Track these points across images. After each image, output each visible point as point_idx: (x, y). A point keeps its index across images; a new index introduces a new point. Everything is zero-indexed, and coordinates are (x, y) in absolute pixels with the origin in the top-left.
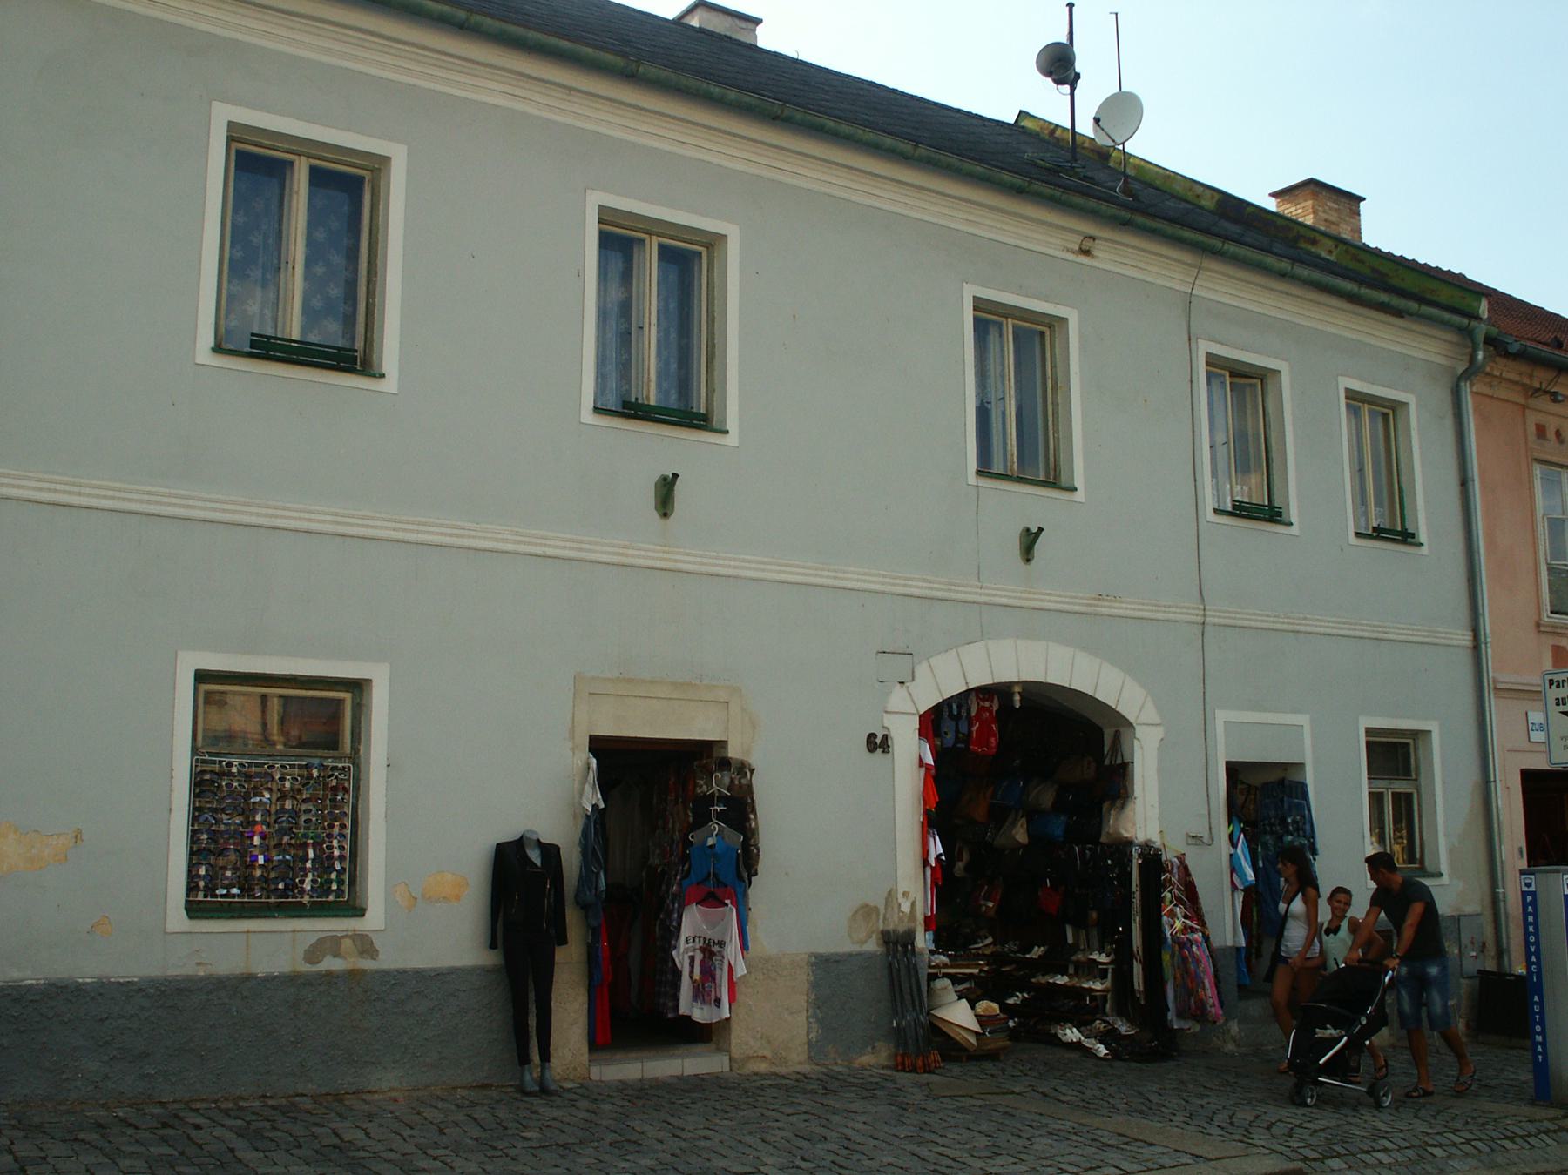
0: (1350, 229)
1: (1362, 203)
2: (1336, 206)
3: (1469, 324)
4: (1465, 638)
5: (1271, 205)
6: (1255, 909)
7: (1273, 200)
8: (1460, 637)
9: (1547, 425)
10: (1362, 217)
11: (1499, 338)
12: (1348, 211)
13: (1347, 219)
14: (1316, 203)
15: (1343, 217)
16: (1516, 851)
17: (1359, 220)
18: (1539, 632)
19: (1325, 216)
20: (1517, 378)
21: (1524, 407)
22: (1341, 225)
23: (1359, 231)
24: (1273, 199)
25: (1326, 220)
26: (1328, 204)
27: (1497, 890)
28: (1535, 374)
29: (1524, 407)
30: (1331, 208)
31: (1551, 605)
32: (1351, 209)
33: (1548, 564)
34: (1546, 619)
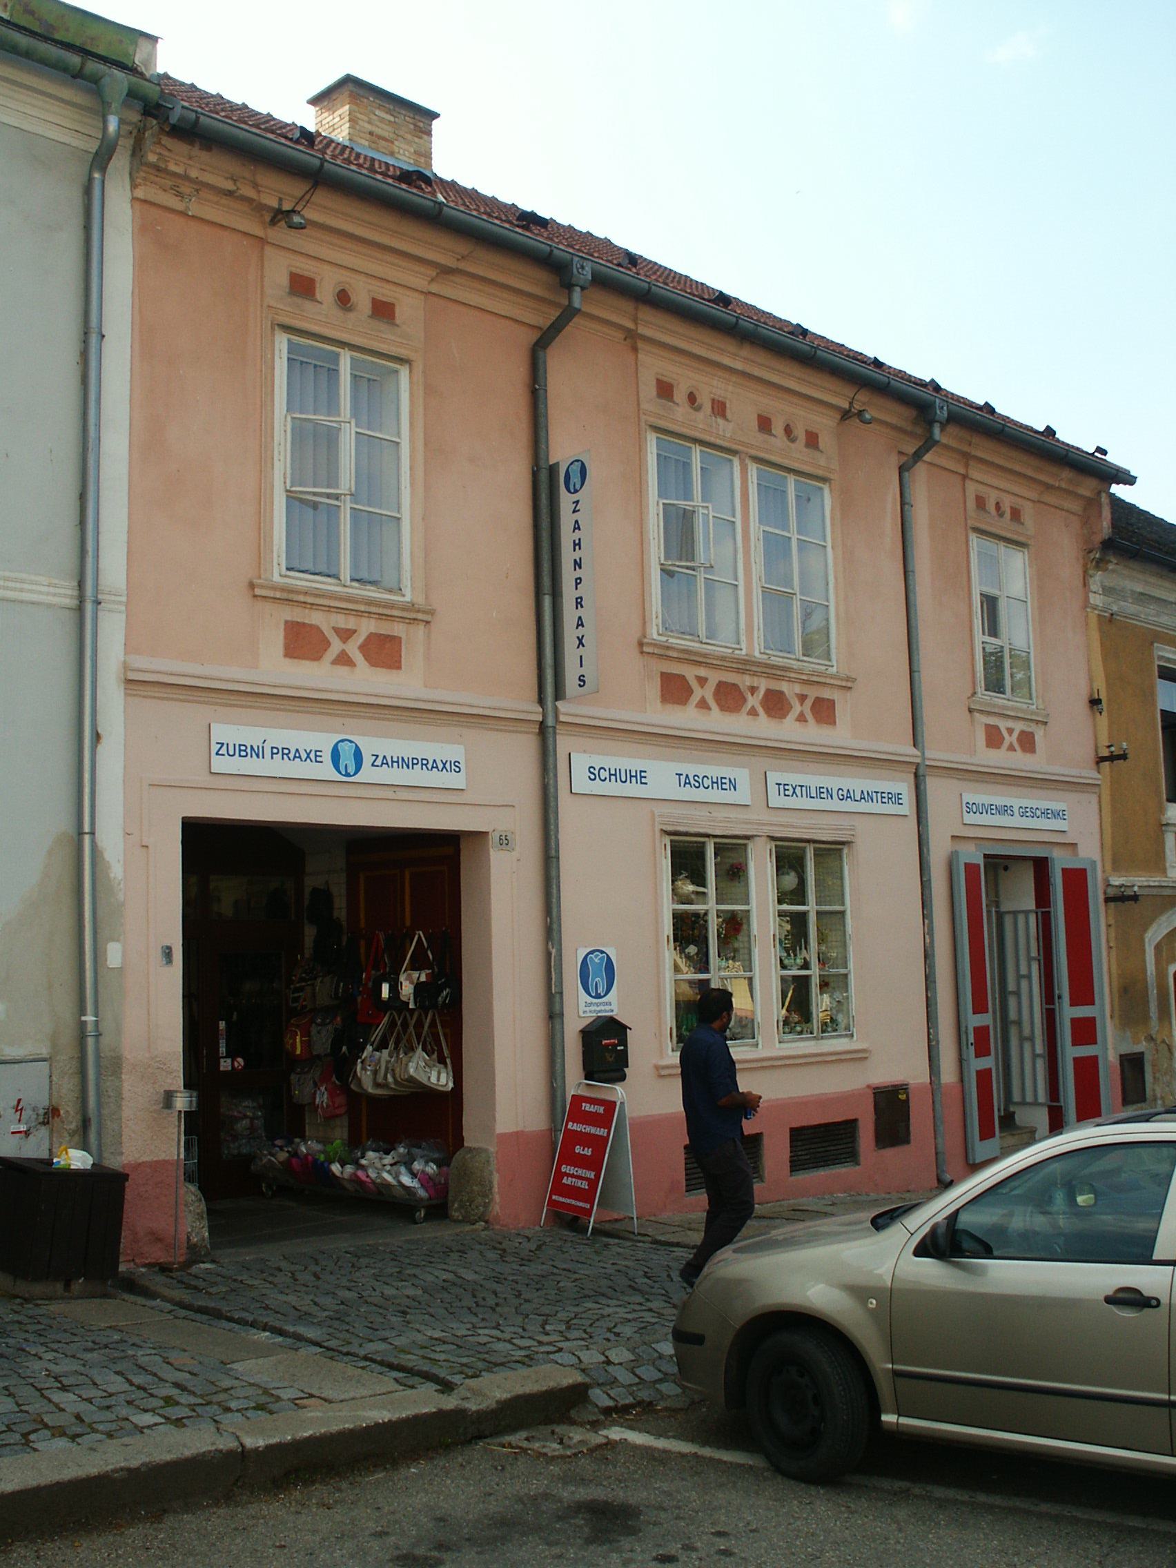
0: (412, 150)
1: (435, 123)
2: (392, 119)
3: (83, 64)
4: (64, 594)
5: (308, 119)
6: (362, 924)
7: (312, 110)
8: (45, 589)
9: (318, 279)
10: (434, 139)
11: (161, 102)
12: (412, 127)
13: (409, 137)
14: (355, 107)
15: (401, 133)
16: (157, 955)
17: (431, 143)
18: (642, 652)
19: (369, 127)
20: (229, 185)
21: (965, 477)
22: (396, 143)
23: (428, 156)
24: (311, 107)
25: (371, 133)
26: (377, 112)
27: (83, 1018)
28: (640, 315)
29: (965, 477)
30: (382, 120)
31: (287, 558)
32: (415, 125)
33: (287, 491)
34: (655, 636)
